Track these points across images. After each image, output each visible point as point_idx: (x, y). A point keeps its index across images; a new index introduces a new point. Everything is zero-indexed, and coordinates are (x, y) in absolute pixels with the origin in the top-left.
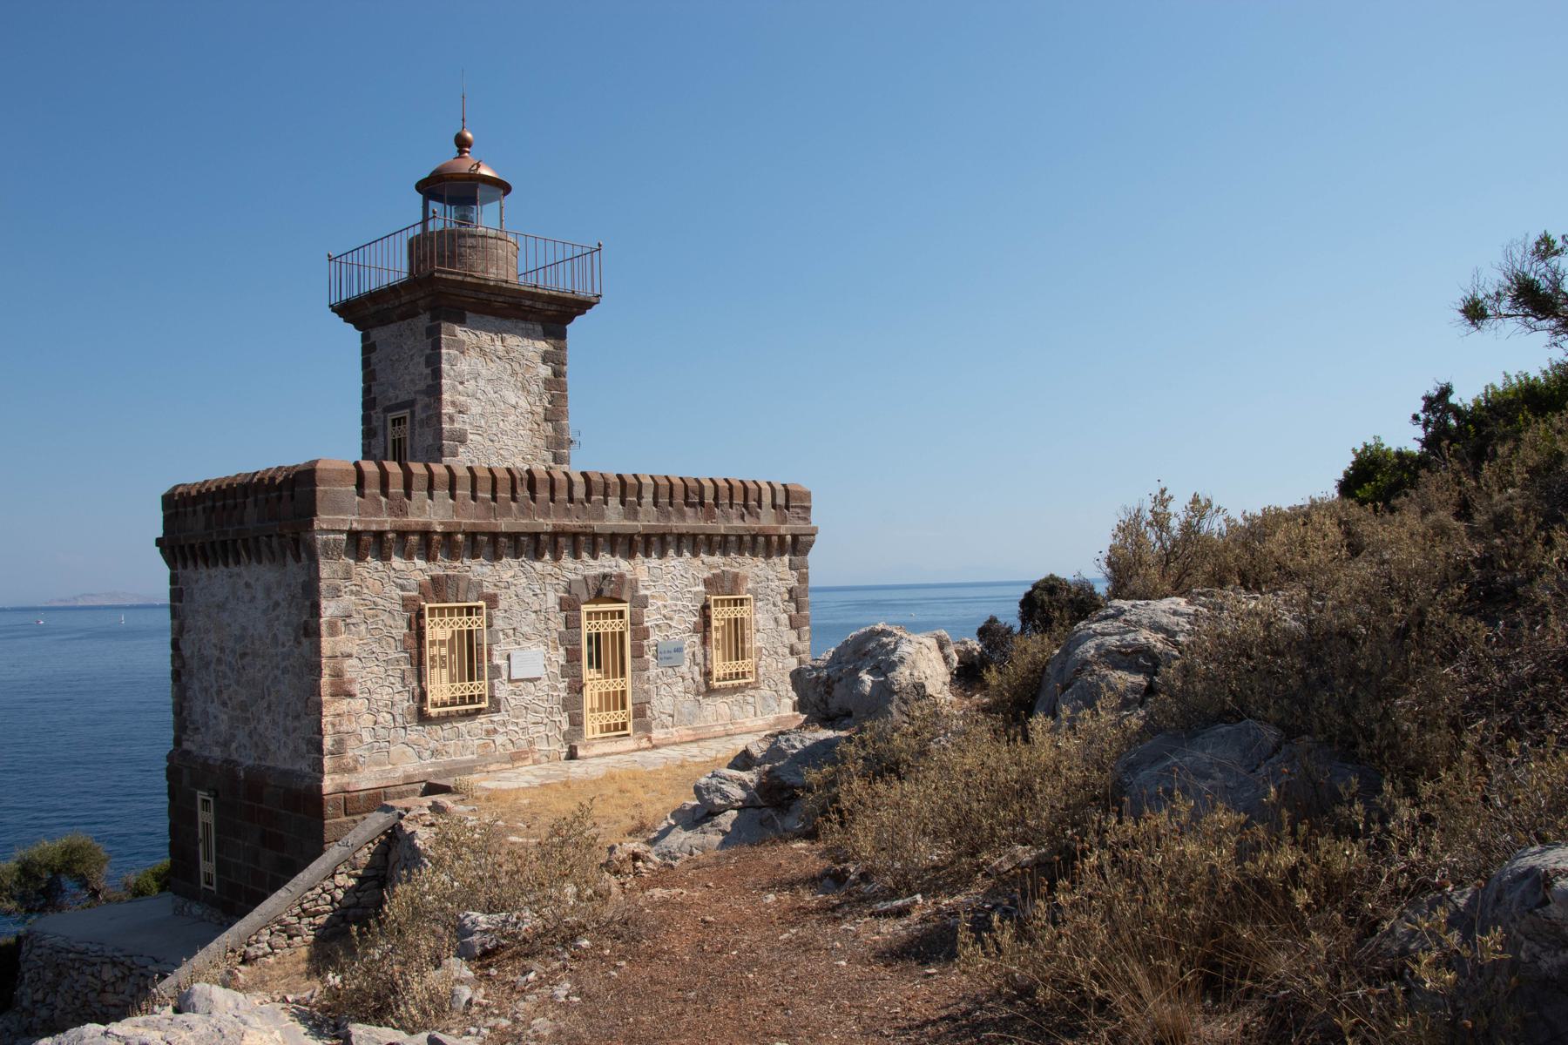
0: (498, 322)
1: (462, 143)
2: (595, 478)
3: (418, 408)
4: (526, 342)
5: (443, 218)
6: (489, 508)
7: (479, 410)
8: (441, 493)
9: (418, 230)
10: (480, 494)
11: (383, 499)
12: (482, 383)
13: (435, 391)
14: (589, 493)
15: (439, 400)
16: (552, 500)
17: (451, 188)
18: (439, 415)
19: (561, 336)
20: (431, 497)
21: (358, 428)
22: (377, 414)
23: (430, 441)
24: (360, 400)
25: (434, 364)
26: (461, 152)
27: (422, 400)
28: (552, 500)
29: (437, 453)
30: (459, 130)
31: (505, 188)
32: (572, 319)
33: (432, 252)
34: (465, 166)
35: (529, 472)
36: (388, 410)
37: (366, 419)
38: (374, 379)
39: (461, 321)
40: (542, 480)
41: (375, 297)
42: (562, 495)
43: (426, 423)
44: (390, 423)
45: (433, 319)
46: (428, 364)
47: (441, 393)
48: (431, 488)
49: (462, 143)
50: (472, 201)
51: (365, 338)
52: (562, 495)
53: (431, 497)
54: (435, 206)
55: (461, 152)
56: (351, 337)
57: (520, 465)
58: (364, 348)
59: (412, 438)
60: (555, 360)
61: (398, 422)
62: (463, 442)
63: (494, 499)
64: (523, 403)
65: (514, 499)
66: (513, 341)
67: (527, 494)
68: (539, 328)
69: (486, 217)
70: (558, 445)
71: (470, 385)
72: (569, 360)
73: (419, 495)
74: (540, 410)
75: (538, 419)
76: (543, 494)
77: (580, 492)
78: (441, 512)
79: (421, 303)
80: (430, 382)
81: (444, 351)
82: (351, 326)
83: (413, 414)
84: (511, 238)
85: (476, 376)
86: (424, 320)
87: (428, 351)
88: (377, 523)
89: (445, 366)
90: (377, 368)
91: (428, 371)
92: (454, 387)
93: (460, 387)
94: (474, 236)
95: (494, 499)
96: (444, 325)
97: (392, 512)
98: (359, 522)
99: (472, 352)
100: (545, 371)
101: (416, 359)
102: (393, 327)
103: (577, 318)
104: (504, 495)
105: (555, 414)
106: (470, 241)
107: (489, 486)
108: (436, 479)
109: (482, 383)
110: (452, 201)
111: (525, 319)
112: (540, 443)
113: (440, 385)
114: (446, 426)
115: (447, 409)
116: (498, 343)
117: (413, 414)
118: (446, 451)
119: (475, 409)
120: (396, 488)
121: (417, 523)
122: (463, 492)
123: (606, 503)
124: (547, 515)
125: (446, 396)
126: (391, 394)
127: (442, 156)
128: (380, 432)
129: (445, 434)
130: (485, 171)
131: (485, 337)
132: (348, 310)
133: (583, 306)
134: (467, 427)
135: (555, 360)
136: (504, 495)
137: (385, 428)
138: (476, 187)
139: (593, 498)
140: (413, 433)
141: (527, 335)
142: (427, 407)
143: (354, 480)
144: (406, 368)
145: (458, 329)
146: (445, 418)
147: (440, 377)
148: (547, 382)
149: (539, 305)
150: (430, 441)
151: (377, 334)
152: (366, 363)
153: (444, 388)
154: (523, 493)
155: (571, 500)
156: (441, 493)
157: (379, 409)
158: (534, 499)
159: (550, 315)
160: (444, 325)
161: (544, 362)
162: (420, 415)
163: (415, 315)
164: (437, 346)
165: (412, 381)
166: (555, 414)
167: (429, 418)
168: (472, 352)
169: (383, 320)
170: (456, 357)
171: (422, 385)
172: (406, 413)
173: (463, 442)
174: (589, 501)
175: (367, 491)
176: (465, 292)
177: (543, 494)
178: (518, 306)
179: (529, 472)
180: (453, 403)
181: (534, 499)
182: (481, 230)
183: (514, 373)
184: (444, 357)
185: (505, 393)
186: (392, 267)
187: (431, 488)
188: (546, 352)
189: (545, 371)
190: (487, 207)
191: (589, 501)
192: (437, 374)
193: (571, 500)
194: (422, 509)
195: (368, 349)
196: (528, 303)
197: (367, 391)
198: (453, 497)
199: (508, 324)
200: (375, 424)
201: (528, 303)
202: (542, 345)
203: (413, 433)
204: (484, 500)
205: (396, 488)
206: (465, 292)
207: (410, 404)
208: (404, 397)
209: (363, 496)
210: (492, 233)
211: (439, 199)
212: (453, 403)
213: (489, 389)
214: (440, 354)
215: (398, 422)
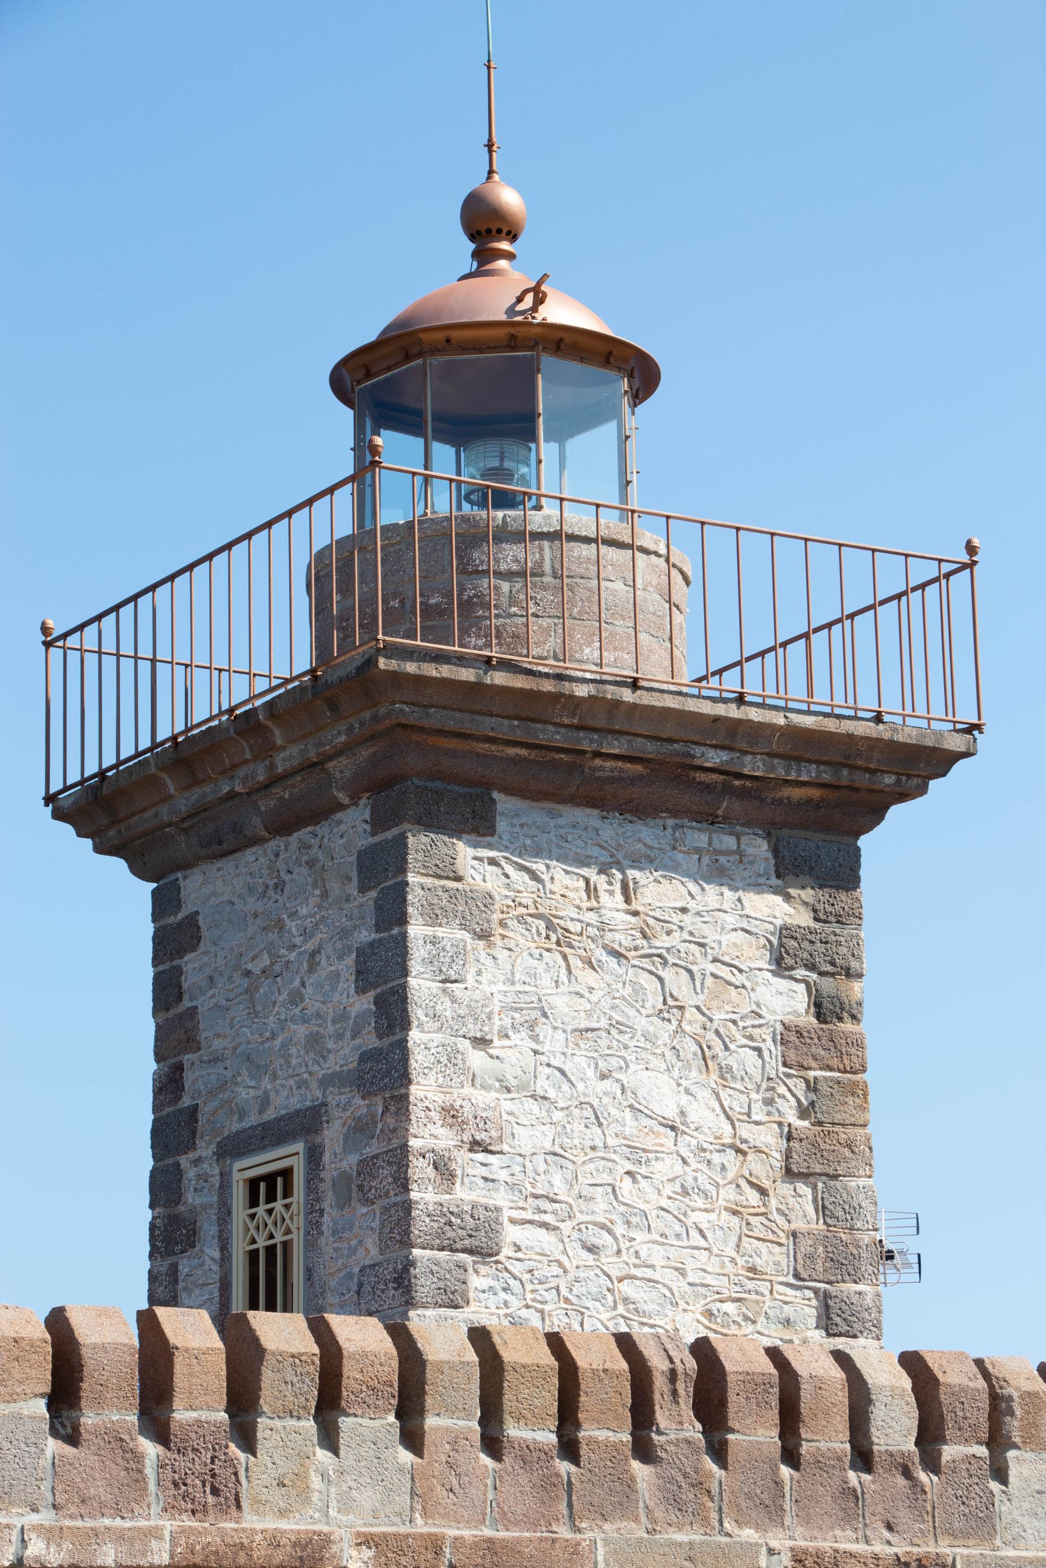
0: (611, 830)
1: (487, 228)
2: (956, 1376)
3: (332, 1136)
4: (712, 895)
5: (422, 479)
6: (549, 1483)
7: (544, 1139)
8: (370, 1426)
9: (338, 519)
10: (514, 1431)
11: (150, 1449)
12: (553, 1041)
13: (386, 1072)
14: (930, 1434)
15: (400, 1104)
16: (791, 1456)
17: (449, 382)
18: (399, 1157)
19: (842, 875)
20: (329, 1439)
21: (136, 1215)
22: (199, 1165)
23: (370, 1250)
24: (146, 1118)
25: (383, 972)
26: (484, 256)
27: (346, 1108)
28: (791, 1456)
29: (389, 1291)
30: (474, 181)
31: (641, 374)
32: (875, 814)
33: (369, 601)
34: (494, 299)
35: (702, 1349)
36: (233, 1148)
37: (164, 1187)
38: (191, 1043)
39: (478, 825)
40: (750, 1379)
41: (186, 756)
42: (827, 1437)
43: (358, 1186)
44: (239, 1194)
45: (378, 824)
46: (364, 980)
47: (405, 1078)
48: (328, 1403)
49: (487, 228)
50: (520, 427)
51: (163, 904)
52: (827, 1437)
53: (329, 1439)
54: (396, 447)
55: (484, 256)
56: (119, 901)
57: (672, 1326)
58: (159, 940)
59: (311, 1245)
60: (821, 960)
61: (268, 1187)
62: (485, 1253)
63: (569, 1449)
64: (704, 1113)
65: (643, 1450)
66: (661, 891)
67: (694, 1431)
68: (759, 848)
69: (571, 473)
70: (839, 1266)
71: (514, 1054)
72: (870, 961)
73: (285, 1428)
74: (768, 1138)
75: (766, 1169)
76: (755, 1433)
77: (895, 1427)
78: (367, 1498)
79: (341, 768)
80: (370, 1041)
81: (416, 930)
82: (118, 865)
83: (314, 1156)
84: (649, 537)
85: (535, 1017)
86: (352, 828)
87: (365, 935)
88: (120, 1537)
89: (420, 984)
90: (203, 1004)
91: (365, 1003)
92: (453, 1056)
93: (476, 1059)
94: (519, 536)
95: (569, 1449)
96: (418, 842)
97: (180, 1494)
98: (50, 1534)
99: (517, 934)
100: (786, 1000)
101: (326, 966)
102: (253, 860)
103: (896, 812)
104: (605, 1431)
105: (821, 1153)
106: (510, 555)
107: (549, 1399)
108: (350, 1371)
109: (553, 1041)
110: (460, 430)
111: (710, 819)
112: (773, 1258)
113: (402, 1049)
114: (424, 1195)
115: (427, 1135)
116: (612, 902)
117: (314, 1156)
118: (424, 1285)
119: (530, 1137)
120: (199, 1403)
121: (274, 1541)
122: (451, 1420)
123: (1000, 1474)
124: (770, 1510)
125: (424, 1090)
126: (245, 1094)
127: (425, 275)
128: (209, 1229)
129: (422, 1224)
130: (560, 311)
131: (563, 881)
132: (102, 810)
133: (917, 765)
134: (501, 1199)
135: (821, 960)
136: (605, 1431)
137: (225, 1212)
138: (532, 370)
139: (949, 1452)
140: (314, 1226)
141: (717, 873)
142: (361, 1129)
143: (42, 1378)
144: (296, 997)
145: (466, 854)
146: (420, 1169)
147: (405, 1024)
148: (790, 1036)
149: (753, 766)
150: (370, 1250)
151: (204, 888)
152: (167, 991)
153: (418, 1060)
154: (677, 1425)
155: (863, 1457)
156: (370, 1426)
157: (205, 1148)
158: (719, 1452)
159: (807, 801)
160: (418, 842)
161: (781, 965)
162: (339, 1159)
163: (321, 812)
164: (392, 913)
165: (314, 1041)
166: (821, 1153)
167: (367, 1167)
168: (517, 934)
169: (220, 837)
170: (460, 952)
171: (343, 1055)
172: (291, 1155)
173: (485, 1253)
174: (932, 1464)
175: (89, 1419)
176: (487, 725)
177: (755, 1433)
178: (683, 771)
179: (702, 1349)
180: (451, 1115)
181: (719, 1452)
182: (544, 517)
183: (670, 1007)
184: (418, 954)
185: (636, 1077)
186: (258, 642)
187: (328, 1403)
188: (786, 932)
189: (786, 1000)
190: (579, 445)
191: (932, 1464)
192: (393, 1012)
193: (863, 1457)
194: (293, 1486)
195: (174, 939)
196: (715, 758)
197: (168, 1086)
198: (412, 1438)
199: (646, 833)
200: (191, 1198)
201: (715, 758)
202: (774, 909)
203: (314, 1226)
204: (529, 1453)
205: (199, 1403)
206: (487, 725)
207: (306, 1123)
208: (286, 1100)
209: (73, 1438)
210: (580, 520)
211: (408, 421)
212: (451, 1115)
213: (579, 1064)
214: (402, 944)
215: (268, 1187)
